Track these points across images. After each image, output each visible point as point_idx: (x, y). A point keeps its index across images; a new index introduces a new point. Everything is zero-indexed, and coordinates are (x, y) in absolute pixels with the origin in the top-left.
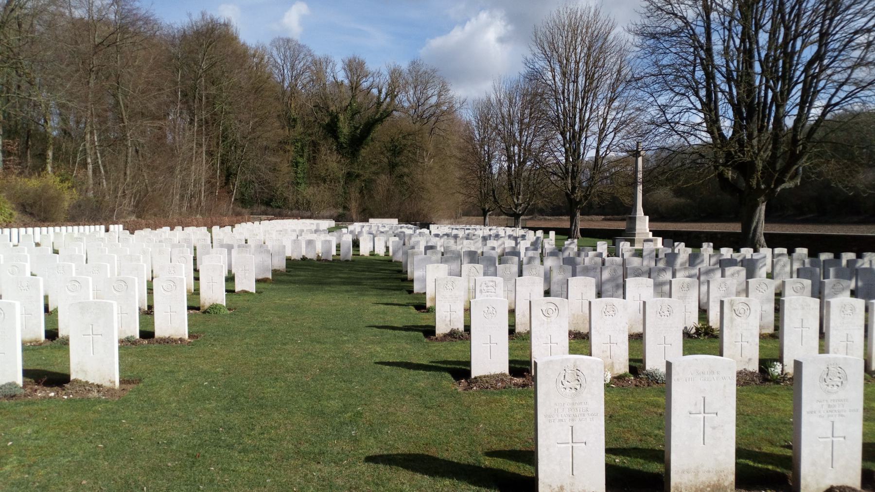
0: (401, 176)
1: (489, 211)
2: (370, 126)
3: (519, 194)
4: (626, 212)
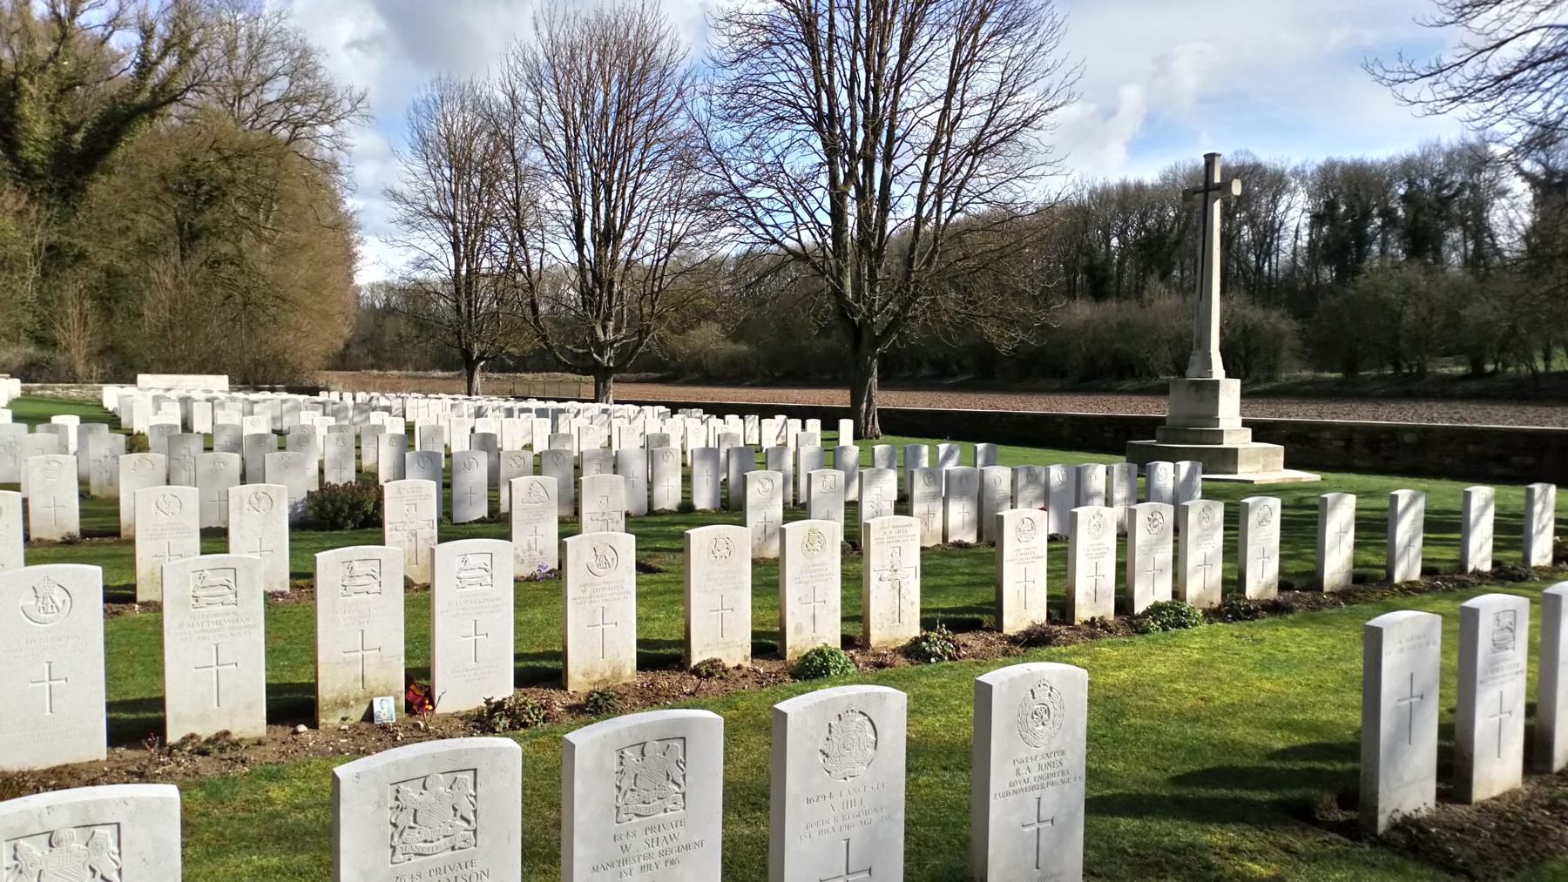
0: (215, 264)
1: (480, 358)
2: (118, 120)
3: (607, 318)
4: (1169, 362)
